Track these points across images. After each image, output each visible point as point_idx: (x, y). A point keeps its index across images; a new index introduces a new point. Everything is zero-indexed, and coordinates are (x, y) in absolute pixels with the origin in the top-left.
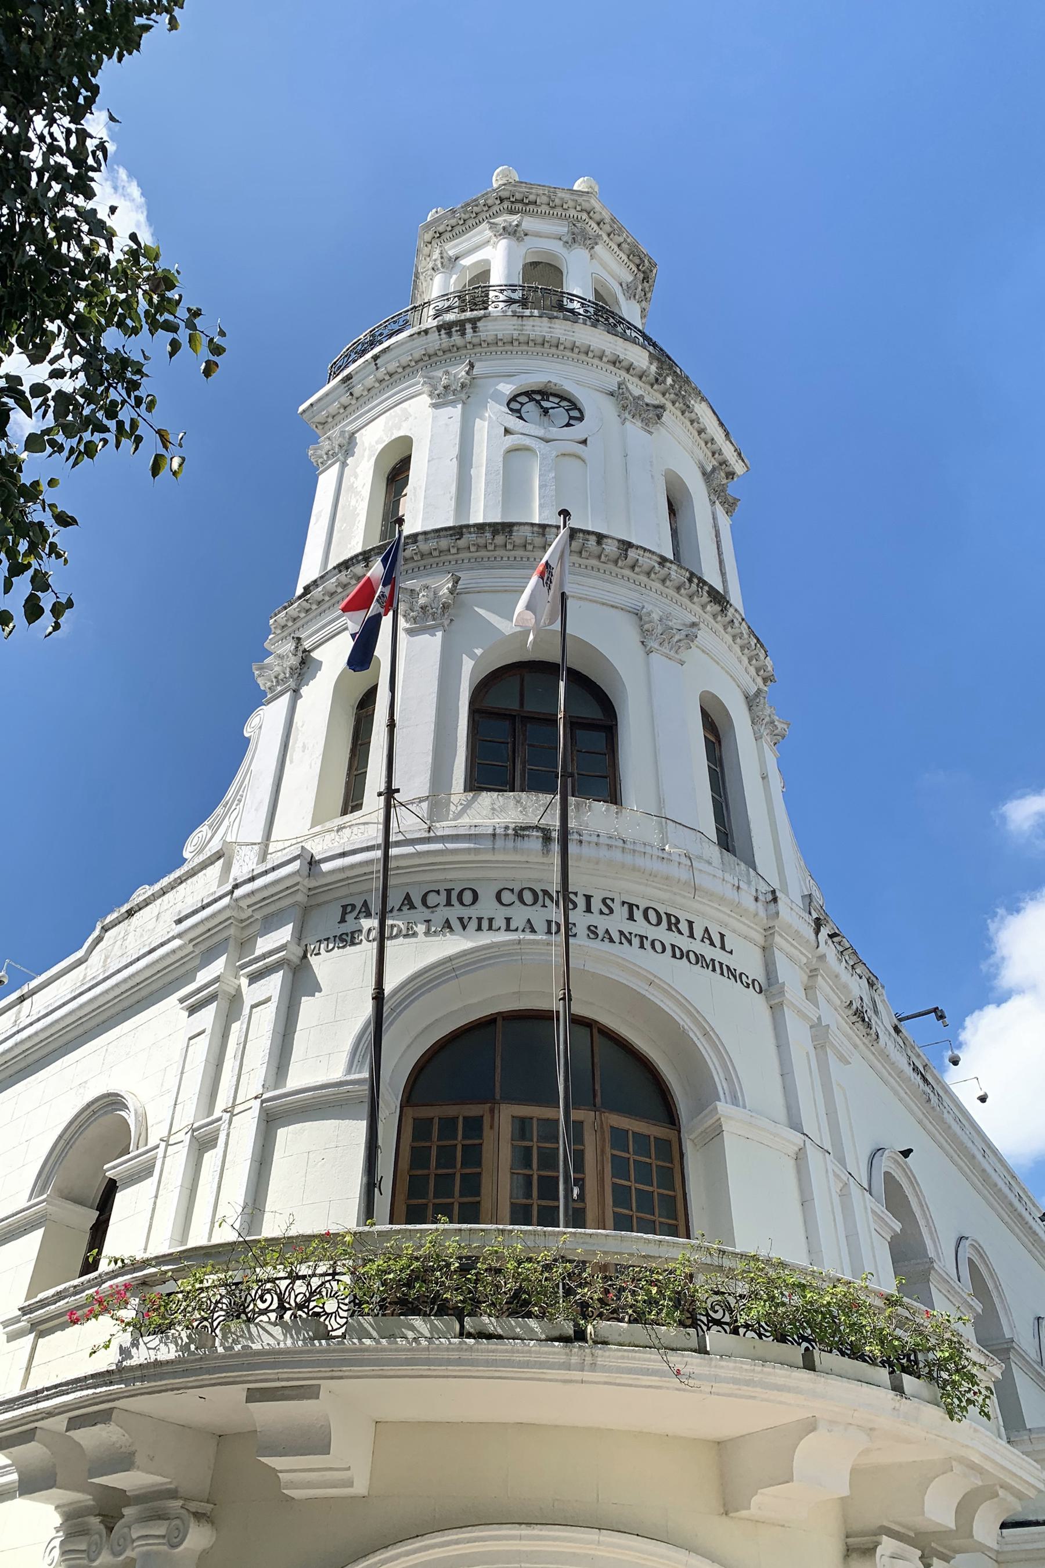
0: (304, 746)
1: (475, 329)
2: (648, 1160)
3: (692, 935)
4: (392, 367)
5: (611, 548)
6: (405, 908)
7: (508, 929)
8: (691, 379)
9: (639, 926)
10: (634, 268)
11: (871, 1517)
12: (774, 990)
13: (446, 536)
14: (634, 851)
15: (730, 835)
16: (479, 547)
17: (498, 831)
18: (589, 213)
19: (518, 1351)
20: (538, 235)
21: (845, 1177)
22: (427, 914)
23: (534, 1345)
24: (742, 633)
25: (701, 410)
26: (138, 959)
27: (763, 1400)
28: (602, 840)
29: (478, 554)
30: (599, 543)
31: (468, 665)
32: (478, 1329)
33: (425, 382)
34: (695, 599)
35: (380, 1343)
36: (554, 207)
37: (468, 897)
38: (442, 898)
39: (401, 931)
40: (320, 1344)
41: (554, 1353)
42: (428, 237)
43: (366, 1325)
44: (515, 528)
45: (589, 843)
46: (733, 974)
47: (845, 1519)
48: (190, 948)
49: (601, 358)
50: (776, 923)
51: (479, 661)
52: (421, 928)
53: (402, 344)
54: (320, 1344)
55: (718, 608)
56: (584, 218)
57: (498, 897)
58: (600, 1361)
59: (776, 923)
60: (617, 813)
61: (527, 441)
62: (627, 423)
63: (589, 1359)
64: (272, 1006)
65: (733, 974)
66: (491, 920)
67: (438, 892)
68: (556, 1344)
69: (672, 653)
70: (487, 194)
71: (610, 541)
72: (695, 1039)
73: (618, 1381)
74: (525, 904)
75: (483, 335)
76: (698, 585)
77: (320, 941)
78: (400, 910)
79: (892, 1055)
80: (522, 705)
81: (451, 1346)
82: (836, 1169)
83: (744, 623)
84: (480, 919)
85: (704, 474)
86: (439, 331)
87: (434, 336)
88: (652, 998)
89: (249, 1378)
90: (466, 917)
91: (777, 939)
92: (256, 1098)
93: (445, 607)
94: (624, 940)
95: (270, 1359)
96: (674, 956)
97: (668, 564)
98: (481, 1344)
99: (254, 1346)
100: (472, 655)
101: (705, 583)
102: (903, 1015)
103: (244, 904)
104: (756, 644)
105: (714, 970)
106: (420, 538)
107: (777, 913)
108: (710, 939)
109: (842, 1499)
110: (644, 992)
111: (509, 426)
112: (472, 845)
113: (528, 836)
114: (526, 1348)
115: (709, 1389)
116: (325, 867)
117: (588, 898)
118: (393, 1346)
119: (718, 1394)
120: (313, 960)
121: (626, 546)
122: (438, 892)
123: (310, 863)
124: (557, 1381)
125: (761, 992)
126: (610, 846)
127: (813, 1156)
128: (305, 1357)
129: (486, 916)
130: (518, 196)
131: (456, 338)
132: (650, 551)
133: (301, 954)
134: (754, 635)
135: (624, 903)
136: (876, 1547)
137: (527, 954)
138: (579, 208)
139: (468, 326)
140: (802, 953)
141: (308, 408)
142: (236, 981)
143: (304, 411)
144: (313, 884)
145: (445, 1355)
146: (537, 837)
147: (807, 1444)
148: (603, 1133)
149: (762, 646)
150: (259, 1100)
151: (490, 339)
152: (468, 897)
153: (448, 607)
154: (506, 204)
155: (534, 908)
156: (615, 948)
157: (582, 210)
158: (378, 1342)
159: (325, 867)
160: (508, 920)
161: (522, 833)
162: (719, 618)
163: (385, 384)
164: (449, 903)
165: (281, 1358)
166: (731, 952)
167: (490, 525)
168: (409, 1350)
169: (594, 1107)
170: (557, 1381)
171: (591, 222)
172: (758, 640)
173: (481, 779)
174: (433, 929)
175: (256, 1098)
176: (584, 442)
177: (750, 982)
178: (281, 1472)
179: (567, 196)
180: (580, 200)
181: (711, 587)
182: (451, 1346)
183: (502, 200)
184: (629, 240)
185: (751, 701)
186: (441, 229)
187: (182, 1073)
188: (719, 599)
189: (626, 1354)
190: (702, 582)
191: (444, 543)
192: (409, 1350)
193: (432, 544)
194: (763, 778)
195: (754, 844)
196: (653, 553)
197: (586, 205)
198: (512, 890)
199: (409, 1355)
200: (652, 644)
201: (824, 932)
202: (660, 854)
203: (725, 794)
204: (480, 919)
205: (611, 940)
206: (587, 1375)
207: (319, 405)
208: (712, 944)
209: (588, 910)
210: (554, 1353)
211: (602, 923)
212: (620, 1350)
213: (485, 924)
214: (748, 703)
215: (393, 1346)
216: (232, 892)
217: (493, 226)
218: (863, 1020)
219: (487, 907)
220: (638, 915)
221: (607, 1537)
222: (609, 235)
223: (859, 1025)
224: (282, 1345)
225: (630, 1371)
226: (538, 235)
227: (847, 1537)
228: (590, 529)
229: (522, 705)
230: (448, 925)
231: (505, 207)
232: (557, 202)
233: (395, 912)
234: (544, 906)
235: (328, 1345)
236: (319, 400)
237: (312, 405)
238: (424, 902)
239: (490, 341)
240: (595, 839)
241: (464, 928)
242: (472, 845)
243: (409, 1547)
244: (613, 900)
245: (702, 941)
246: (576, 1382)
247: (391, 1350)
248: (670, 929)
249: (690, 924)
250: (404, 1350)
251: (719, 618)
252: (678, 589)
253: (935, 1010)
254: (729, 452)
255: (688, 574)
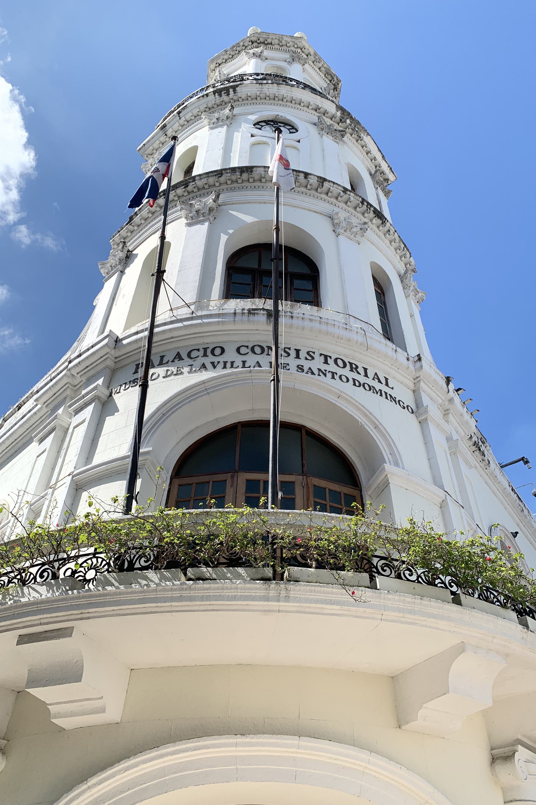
0: (124, 296)
1: (235, 91)
2: (340, 506)
3: (366, 375)
4: (188, 117)
5: (313, 181)
6: (176, 360)
7: (244, 367)
8: (360, 122)
9: (331, 367)
10: (328, 82)
11: (507, 732)
12: (421, 411)
13: (211, 176)
14: (327, 323)
15: (389, 329)
16: (233, 182)
17: (237, 311)
18: (301, 49)
19: (227, 588)
20: (273, 59)
21: (475, 527)
22: (191, 362)
23: (240, 583)
24: (395, 239)
25: (367, 140)
26: (16, 424)
27: (423, 626)
28: (305, 316)
29: (232, 185)
30: (306, 177)
31: (224, 238)
32: (198, 575)
33: (206, 118)
34: (366, 215)
35: (119, 588)
36: (281, 45)
37: (218, 351)
38: (202, 352)
39: (173, 372)
40: (73, 593)
41: (256, 589)
42: (212, 66)
43: (111, 579)
44: (254, 169)
45: (298, 318)
46: (393, 399)
47: (490, 737)
48: (45, 410)
49: (308, 107)
50: (420, 374)
51: (231, 236)
52: (186, 370)
53: (194, 103)
54: (73, 593)
55: (380, 222)
56: (299, 51)
57: (238, 350)
58: (292, 594)
59: (420, 374)
60: (317, 311)
61: (264, 139)
62: (324, 137)
63: (283, 593)
64: (86, 424)
65: (393, 399)
66: (232, 363)
67: (198, 350)
68: (258, 582)
69: (352, 236)
70: (244, 40)
71: (312, 177)
72: (369, 430)
73: (307, 610)
74: (256, 354)
75: (239, 95)
76: (367, 207)
77: (121, 386)
78: (173, 361)
79: (498, 477)
80: (260, 265)
81: (174, 587)
82: (468, 520)
83: (396, 233)
84: (225, 363)
85: (371, 175)
86: (214, 94)
87: (211, 97)
88: (340, 405)
89: (18, 626)
90: (216, 362)
91: (422, 384)
92: (69, 475)
93: (211, 210)
94: (321, 374)
95: (34, 608)
96: (355, 384)
97: (348, 193)
98: (198, 584)
99: (23, 600)
100: (226, 233)
101: (371, 206)
102: (503, 464)
103: (74, 372)
104: (404, 248)
105: (381, 395)
106: (197, 178)
107: (421, 367)
108: (378, 379)
109: (485, 713)
110: (334, 402)
111: (253, 133)
112: (220, 320)
113: (257, 313)
114: (234, 585)
115: (380, 617)
116: (125, 342)
117: (298, 351)
118: (129, 590)
119: (387, 620)
120: (115, 397)
121: (322, 180)
122: (198, 350)
123: (116, 341)
124: (259, 611)
125: (413, 412)
126: (311, 320)
127: (453, 508)
128: (61, 604)
129: (229, 360)
130: (262, 40)
131: (225, 98)
132: (337, 184)
133: (108, 394)
134: (403, 242)
135: (321, 355)
136: (514, 753)
137: (256, 379)
138: (296, 46)
139: (231, 90)
140: (439, 396)
141: (142, 147)
142: (70, 420)
143: (140, 149)
144: (118, 353)
145: (169, 594)
146: (263, 314)
147: (460, 664)
148: (308, 488)
149: (408, 250)
150: (71, 476)
151: (244, 97)
152: (218, 351)
153: (213, 210)
154: (255, 44)
155: (262, 356)
156: (316, 377)
157: (297, 48)
158: (117, 588)
159: (125, 342)
160: (244, 362)
161: (253, 312)
162: (381, 228)
163: (185, 127)
164: (205, 355)
165: (43, 607)
166: (393, 388)
167: (239, 168)
168: (141, 592)
169: (303, 473)
170: (259, 611)
171: (303, 54)
172: (405, 246)
173: (229, 293)
174: (194, 369)
175: (69, 475)
176: (299, 141)
177: (405, 406)
178: (50, 705)
179: (289, 39)
180: (296, 41)
181: (375, 208)
182: (174, 587)
183: (253, 43)
184: (325, 66)
185: (402, 278)
186: (220, 61)
187: (30, 476)
188: (379, 214)
189: (313, 588)
190: (369, 205)
191: (211, 180)
192: (141, 592)
193: (204, 181)
194: (411, 316)
195: (406, 343)
196: (339, 185)
197: (300, 45)
198: (247, 347)
199: (141, 596)
200: (340, 231)
201: (452, 386)
202: (345, 326)
203: (387, 317)
204: (225, 363)
205: (313, 373)
206: (283, 605)
207: (148, 144)
208: (380, 381)
209: (298, 357)
210: (256, 589)
211: (307, 365)
212: (308, 585)
213: (229, 365)
214: (401, 279)
215: (129, 590)
216: (67, 366)
217: (247, 53)
218: (480, 450)
219: (230, 355)
220: (330, 361)
221: (306, 742)
222: (313, 62)
223: (477, 452)
224: (43, 597)
225: (317, 601)
226: (273, 59)
227: (492, 750)
228: (301, 170)
229: (260, 265)
230: (204, 366)
231: (255, 46)
232: (284, 43)
233: (170, 363)
234: (268, 354)
235: (79, 593)
236: (148, 141)
237: (144, 145)
238: (189, 355)
239: (244, 98)
240: (302, 316)
241: (215, 367)
242: (220, 320)
243: (148, 756)
244: (314, 353)
245: (373, 379)
246: (274, 611)
247: (127, 593)
248: (351, 370)
249: (365, 370)
250: (137, 593)
251: (381, 228)
252: (355, 208)
253: (523, 459)
254: (384, 167)
255: (361, 199)
